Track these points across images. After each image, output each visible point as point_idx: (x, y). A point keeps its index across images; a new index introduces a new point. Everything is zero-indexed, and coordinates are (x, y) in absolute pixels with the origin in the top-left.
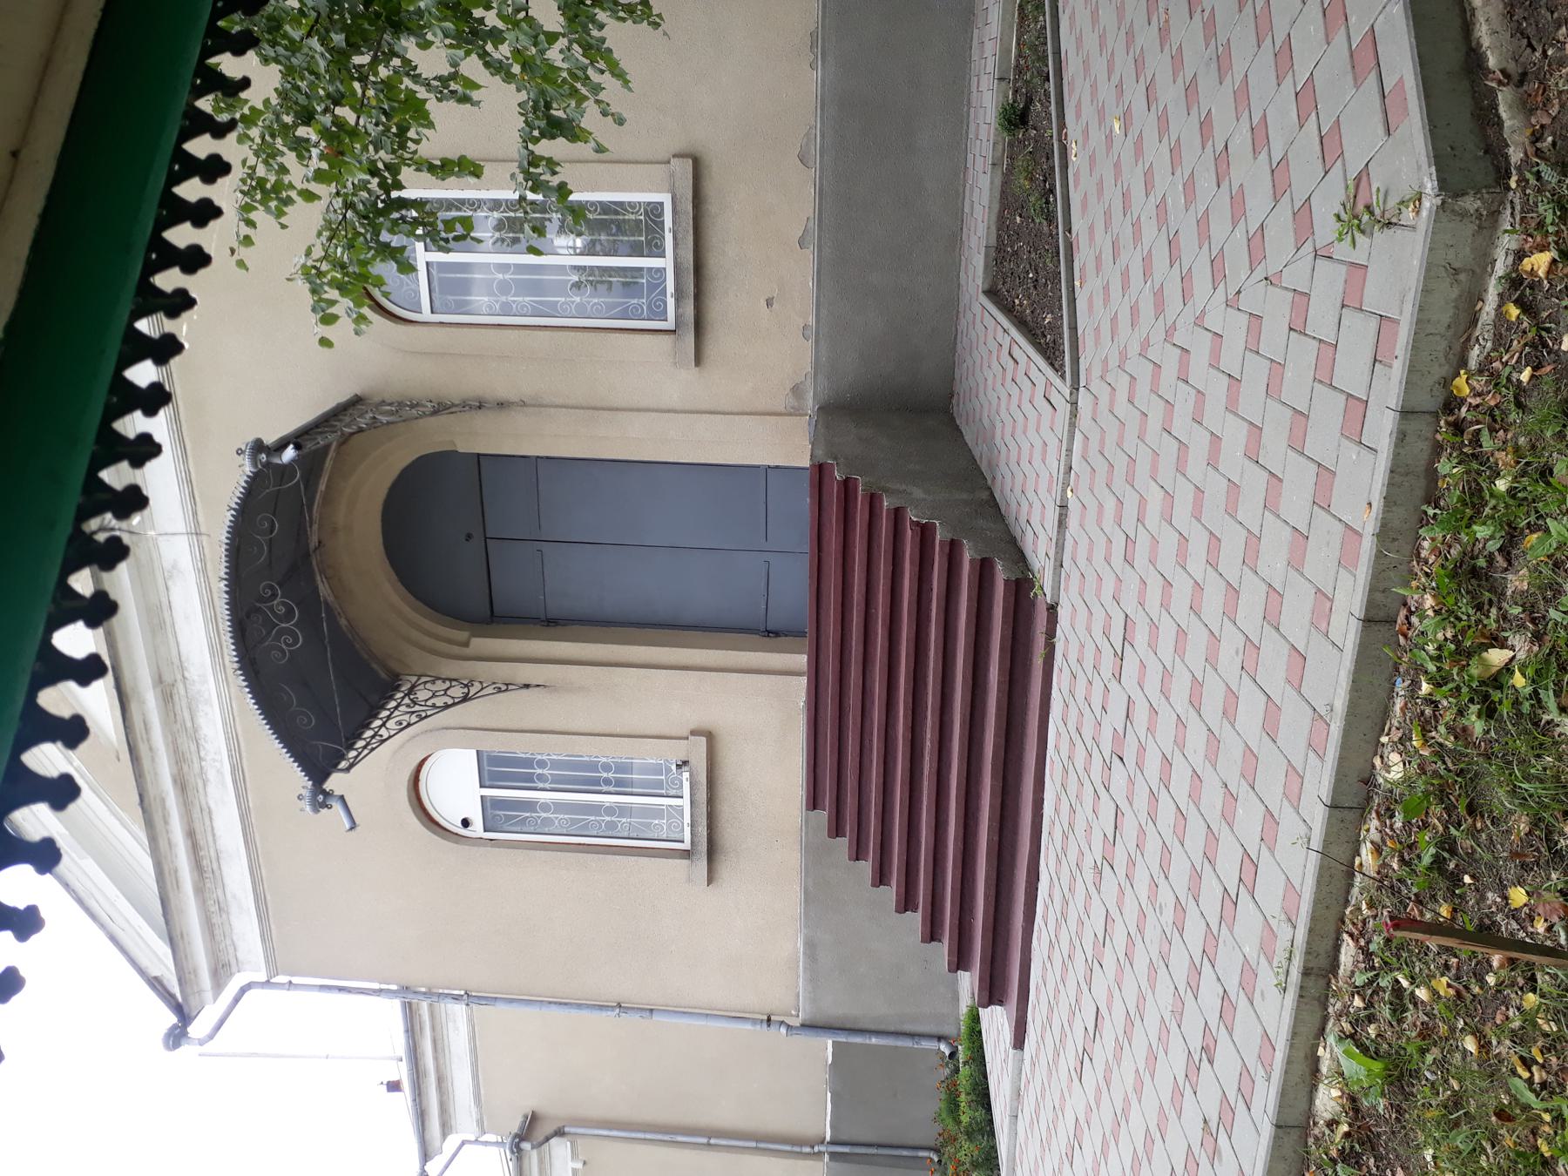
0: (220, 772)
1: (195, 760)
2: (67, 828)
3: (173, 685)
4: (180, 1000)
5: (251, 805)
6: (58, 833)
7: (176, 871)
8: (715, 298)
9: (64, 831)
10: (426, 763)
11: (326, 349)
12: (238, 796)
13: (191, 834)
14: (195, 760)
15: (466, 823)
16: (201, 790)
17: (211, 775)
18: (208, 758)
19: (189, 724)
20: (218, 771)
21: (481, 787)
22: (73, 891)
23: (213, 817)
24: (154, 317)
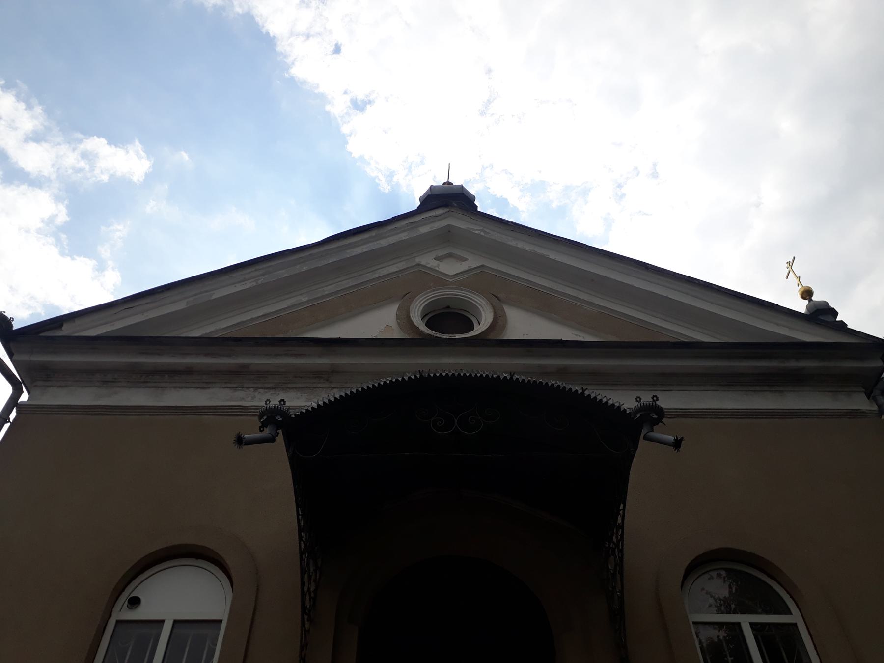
0: (242, 399)
1: (256, 386)
2: (214, 299)
3: (327, 380)
4: (41, 335)
5: (204, 417)
6: (214, 293)
7: (159, 354)
8: (67, 215)
9: (214, 297)
10: (229, 584)
11: (343, 48)
12: (215, 407)
13: (189, 371)
14: (256, 386)
15: (135, 602)
16: (226, 385)
17: (240, 394)
18: (256, 394)
19: (290, 386)
20: (243, 399)
21: (175, 622)
22: (163, 291)
23: (199, 390)
24: (666, 413)
